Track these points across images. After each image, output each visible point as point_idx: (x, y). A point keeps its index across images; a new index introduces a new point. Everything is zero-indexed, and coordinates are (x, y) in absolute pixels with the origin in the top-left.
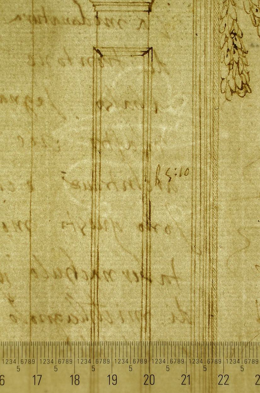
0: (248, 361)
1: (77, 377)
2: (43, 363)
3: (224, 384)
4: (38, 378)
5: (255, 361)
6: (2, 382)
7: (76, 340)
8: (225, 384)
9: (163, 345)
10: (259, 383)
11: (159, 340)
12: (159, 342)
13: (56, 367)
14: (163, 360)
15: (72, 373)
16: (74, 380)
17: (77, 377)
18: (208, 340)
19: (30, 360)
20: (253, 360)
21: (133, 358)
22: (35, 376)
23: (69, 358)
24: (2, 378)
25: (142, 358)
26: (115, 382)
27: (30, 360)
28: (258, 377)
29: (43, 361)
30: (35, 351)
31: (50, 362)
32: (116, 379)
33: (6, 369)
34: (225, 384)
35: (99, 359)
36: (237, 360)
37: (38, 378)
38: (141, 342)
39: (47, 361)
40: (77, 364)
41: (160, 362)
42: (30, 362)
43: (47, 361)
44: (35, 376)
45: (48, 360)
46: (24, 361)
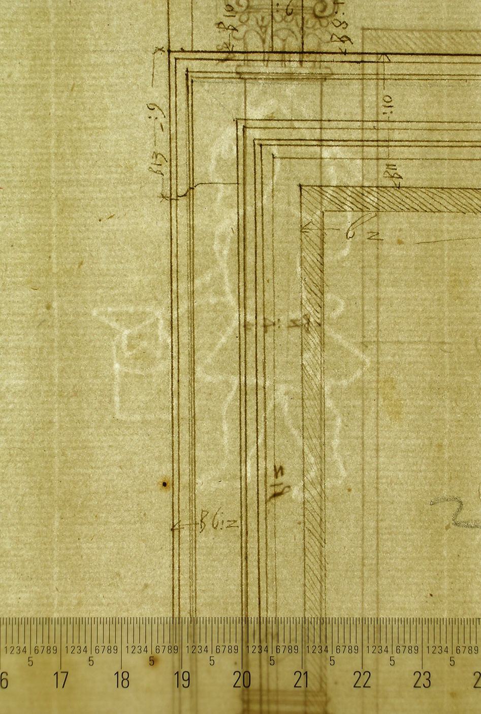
0: (222, 649)
1: (125, 676)
2: (70, 651)
3: (362, 687)
4: (62, 677)
5: (233, 649)
6: (4, 683)
7: (422, 615)
8: (364, 687)
9: (47, 623)
10: (479, 685)
11: (141, 615)
12: (352, 619)
13: (30, 659)
14: (22, 648)
15: (117, 668)
16: (120, 679)
17: (125, 676)
18: (370, 614)
19: (49, 648)
20: (230, 648)
21: (215, 644)
22: (57, 673)
23: (353, 644)
24: (4, 676)
25: (231, 644)
26: (186, 684)
27: (109, 648)
28: (478, 675)
29: (431, 649)
30: (15, 635)
31: (142, 651)
32: (189, 679)
33: (11, 664)
34: (364, 687)
35: (100, 646)
36: (323, 649)
37: (62, 677)
38: (246, 620)
39: (137, 650)
40: (426, 654)
41: (380, 651)
42: (49, 652)
43: (137, 650)
44: (57, 673)
45: (140, 648)
46: (101, 649)
